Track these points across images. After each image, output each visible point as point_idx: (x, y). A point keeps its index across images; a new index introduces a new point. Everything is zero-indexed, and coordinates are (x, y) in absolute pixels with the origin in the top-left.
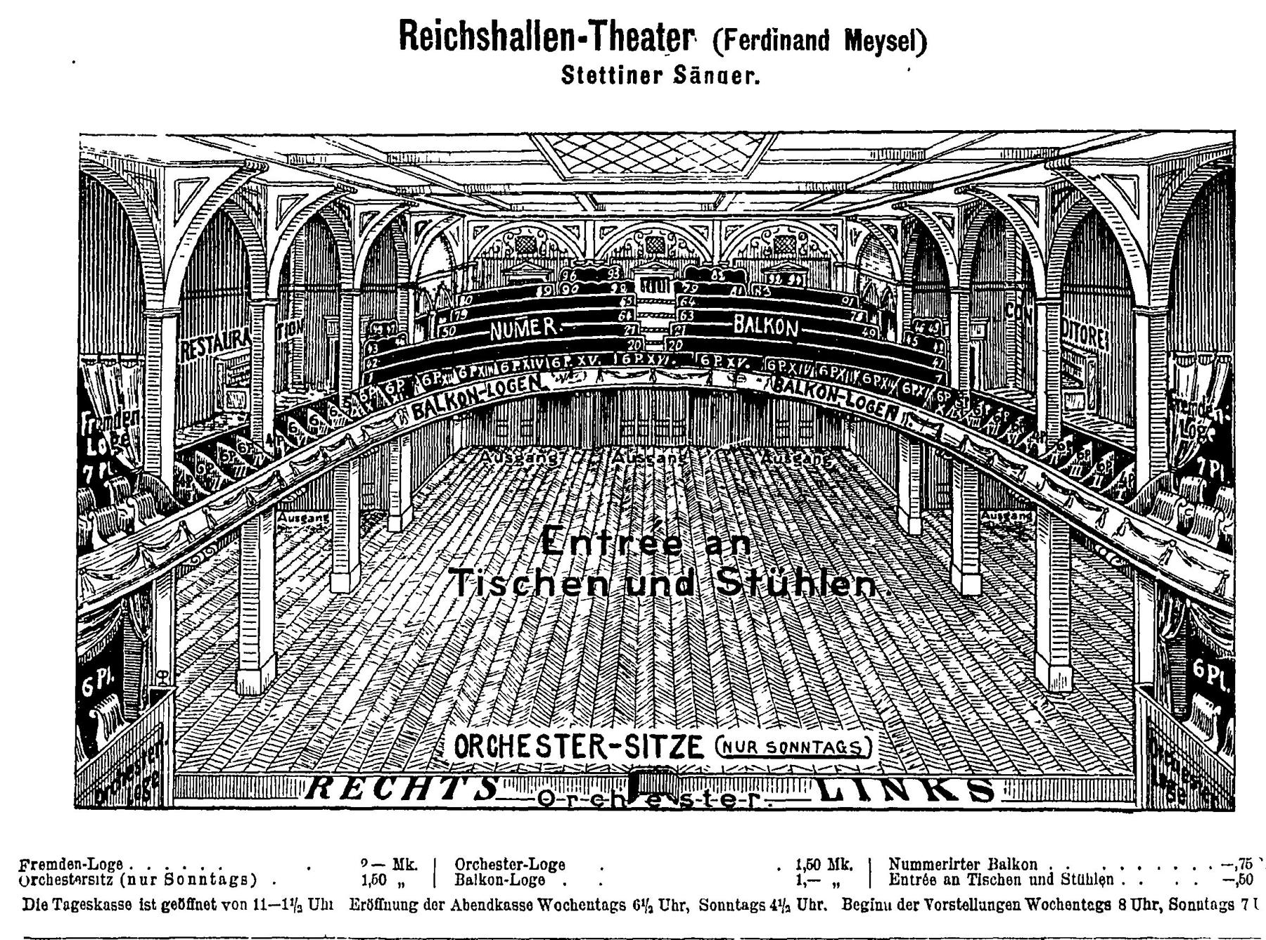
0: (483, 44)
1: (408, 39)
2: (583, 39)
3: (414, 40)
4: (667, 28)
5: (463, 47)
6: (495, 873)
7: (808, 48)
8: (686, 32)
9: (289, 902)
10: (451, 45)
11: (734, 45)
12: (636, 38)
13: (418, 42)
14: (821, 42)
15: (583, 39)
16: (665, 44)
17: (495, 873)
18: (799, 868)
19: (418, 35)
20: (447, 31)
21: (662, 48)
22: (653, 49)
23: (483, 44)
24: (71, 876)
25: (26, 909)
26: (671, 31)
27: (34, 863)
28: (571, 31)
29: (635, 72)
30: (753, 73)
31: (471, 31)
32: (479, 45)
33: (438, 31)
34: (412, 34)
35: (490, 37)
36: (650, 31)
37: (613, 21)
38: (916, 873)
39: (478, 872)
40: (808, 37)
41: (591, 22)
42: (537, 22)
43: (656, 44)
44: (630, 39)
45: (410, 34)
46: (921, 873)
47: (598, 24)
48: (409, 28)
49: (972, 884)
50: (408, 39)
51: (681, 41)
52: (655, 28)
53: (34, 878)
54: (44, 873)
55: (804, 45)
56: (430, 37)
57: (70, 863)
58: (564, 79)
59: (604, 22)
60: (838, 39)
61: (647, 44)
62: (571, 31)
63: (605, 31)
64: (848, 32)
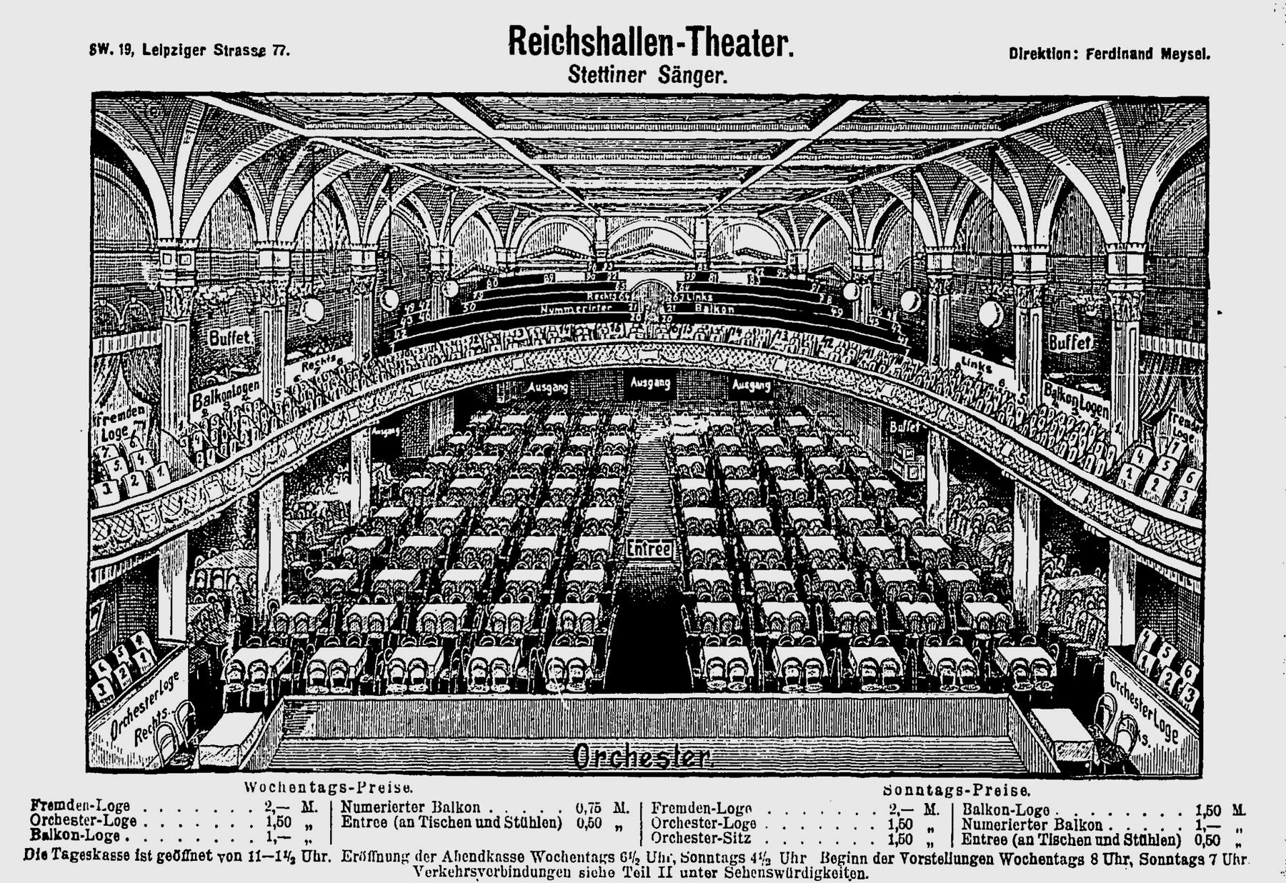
1: (517, 45)
2: (681, 45)
3: (522, 45)
4: (761, 35)
5: (569, 52)
7: (632, 54)
9: (282, 854)
11: (1092, 57)
12: (732, 43)
13: (526, 48)
14: (1149, 54)
15: (681, 45)
16: (760, 50)
19: (526, 40)
21: (757, 54)
22: (748, 54)
23: (588, 40)
26: (765, 37)
28: (670, 38)
30: (722, 73)
31: (576, 36)
32: (584, 51)
33: (547, 36)
34: (520, 40)
35: (595, 43)
36: (746, 38)
37: (709, 28)
38: (367, 816)
40: (662, 38)
41: (688, 28)
42: (640, 28)
43: (752, 50)
44: (724, 45)
46: (373, 815)
47: (695, 29)
48: (517, 33)
49: (423, 826)
50: (517, 45)
51: (658, 47)
52: (750, 34)
55: (627, 49)
58: (660, 79)
59: (701, 28)
60: (1157, 53)
61: (743, 50)
62: (670, 38)
63: (702, 36)
64: (1163, 50)
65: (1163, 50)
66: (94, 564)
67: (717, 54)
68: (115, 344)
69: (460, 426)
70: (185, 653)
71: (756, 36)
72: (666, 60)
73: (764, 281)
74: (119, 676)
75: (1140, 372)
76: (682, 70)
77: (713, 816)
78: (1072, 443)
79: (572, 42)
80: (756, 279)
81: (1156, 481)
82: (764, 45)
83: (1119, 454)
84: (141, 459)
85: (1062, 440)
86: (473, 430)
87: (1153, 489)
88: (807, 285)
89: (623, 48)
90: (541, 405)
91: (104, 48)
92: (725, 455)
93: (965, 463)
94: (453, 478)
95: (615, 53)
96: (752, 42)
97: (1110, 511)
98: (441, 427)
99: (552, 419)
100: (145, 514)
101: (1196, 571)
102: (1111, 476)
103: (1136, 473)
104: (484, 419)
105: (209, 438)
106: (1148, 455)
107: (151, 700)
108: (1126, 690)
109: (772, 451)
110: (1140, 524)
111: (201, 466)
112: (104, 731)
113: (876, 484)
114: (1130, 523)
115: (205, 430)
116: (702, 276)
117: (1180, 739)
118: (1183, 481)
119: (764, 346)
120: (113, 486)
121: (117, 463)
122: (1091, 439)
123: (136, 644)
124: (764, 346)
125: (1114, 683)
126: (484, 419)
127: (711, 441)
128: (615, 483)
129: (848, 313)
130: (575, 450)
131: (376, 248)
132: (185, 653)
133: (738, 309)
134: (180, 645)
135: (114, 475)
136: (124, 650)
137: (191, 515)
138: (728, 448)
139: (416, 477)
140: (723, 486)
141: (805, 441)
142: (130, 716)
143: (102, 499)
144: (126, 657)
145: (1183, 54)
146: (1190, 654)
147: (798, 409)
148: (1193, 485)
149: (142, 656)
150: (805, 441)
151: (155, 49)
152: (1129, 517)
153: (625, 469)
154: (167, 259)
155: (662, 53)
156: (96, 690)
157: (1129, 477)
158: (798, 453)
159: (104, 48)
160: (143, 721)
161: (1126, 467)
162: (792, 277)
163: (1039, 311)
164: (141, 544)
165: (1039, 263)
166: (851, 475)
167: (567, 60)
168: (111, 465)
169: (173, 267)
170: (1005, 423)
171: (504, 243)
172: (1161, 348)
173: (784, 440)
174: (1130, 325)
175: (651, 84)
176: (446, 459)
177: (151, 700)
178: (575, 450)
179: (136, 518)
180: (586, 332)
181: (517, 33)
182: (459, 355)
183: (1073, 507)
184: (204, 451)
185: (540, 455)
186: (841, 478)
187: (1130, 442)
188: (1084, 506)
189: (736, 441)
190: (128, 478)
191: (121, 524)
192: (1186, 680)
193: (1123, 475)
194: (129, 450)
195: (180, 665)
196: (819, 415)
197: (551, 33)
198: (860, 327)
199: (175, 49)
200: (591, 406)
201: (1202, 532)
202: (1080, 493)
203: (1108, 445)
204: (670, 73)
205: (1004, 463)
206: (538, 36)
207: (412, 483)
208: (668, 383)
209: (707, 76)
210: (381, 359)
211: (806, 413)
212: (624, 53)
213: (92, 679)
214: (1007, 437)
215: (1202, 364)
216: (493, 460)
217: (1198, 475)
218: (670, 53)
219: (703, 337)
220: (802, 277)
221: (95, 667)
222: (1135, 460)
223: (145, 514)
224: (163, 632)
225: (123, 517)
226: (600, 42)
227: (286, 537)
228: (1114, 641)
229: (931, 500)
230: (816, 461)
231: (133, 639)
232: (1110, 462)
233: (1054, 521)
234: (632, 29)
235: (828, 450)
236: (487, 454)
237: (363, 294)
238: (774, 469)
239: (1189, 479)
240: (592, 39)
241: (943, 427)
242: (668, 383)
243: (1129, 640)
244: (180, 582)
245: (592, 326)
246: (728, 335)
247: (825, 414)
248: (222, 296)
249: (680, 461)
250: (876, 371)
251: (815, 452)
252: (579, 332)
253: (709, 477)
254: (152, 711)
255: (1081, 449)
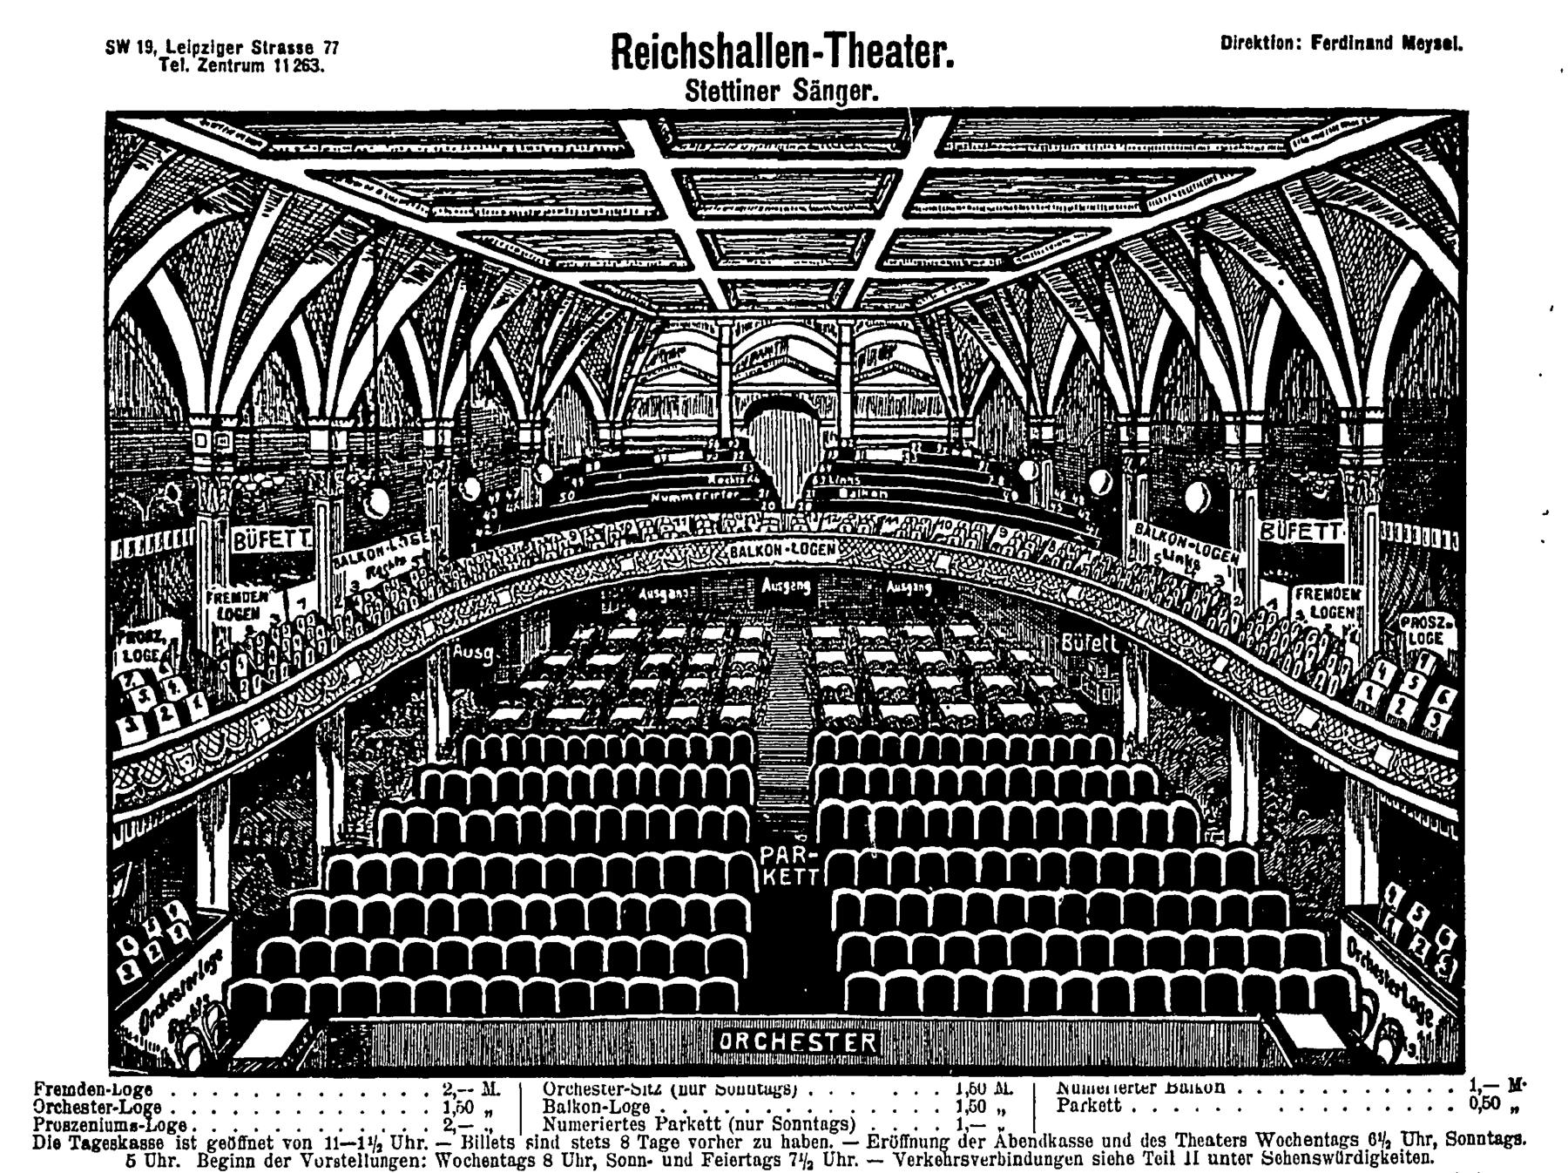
0: (707, 61)
1: (621, 57)
2: (818, 55)
3: (627, 56)
4: (915, 41)
5: (684, 66)
6: (591, 1099)
7: (759, 65)
8: (937, 45)
10: (670, 61)
11: (1320, 46)
12: (880, 52)
13: (633, 60)
14: (1388, 44)
15: (818, 55)
17: (591, 1099)
18: (960, 1093)
19: (632, 51)
20: (666, 46)
21: (910, 65)
23: (707, 61)
24: (94, 1103)
25: (36, 1147)
27: (49, 1087)
28: (805, 46)
29: (752, 87)
31: (692, 45)
32: (701, 62)
33: (655, 46)
34: (625, 51)
35: (714, 53)
36: (898, 45)
37: (853, 34)
39: (571, 1098)
40: (796, 45)
41: (827, 35)
42: (769, 35)
44: (871, 54)
45: (1227, 43)
47: (834, 36)
48: (622, 43)
50: (621, 57)
52: (902, 40)
53: (50, 1105)
54: (59, 1100)
55: (754, 60)
56: (646, 55)
57: (91, 1089)
59: (843, 34)
60: (1398, 42)
61: (894, 60)
62: (805, 46)
63: (844, 43)
64: (1405, 37)
65: (1405, 37)
66: (117, 818)
67: (769, 65)
68: (140, 545)
69: (559, 645)
70: (229, 929)
71: (909, 44)
72: (800, 72)
73: (921, 459)
74: (149, 954)
75: (1381, 568)
76: (821, 85)
77: (108, 1098)
78: (1297, 655)
79: (686, 51)
80: (912, 456)
81: (1402, 702)
82: (919, 54)
83: (1356, 668)
84: (172, 686)
85: (1286, 652)
86: (575, 648)
87: (1398, 712)
88: (973, 463)
89: (749, 58)
90: (654, 617)
91: (124, 46)
92: (878, 674)
93: (1173, 686)
94: (550, 708)
95: (740, 65)
96: (904, 50)
97: (1345, 739)
98: (535, 644)
99: (668, 633)
100: (179, 756)
101: (1451, 814)
102: (1346, 695)
103: (1377, 692)
104: (587, 634)
105: (255, 661)
106: (1391, 669)
107: (190, 983)
108: (1370, 962)
109: (934, 669)
110: (1384, 756)
111: (245, 696)
112: (132, 1023)
113: (1062, 708)
114: (1372, 753)
115: (251, 652)
116: (847, 453)
117: (1435, 1021)
118: (1434, 702)
119: (924, 539)
120: (139, 720)
121: (143, 693)
122: (1323, 650)
123: (171, 916)
124: (924, 539)
125: (1354, 953)
126: (587, 634)
127: (861, 657)
128: (745, 711)
129: (1025, 497)
130: (695, 670)
131: (452, 424)
132: (229, 929)
133: (892, 494)
134: (223, 916)
135: (139, 707)
136: (156, 923)
137: (233, 757)
138: (883, 665)
139: (505, 706)
140: (877, 712)
141: (975, 656)
142: (165, 1004)
143: (126, 738)
144: (157, 932)
145: (1429, 43)
146: (1448, 904)
147: (963, 617)
148: (1446, 707)
149: (178, 930)
150: (975, 656)
151: (181, 46)
152: (1370, 747)
153: (758, 693)
154: (201, 441)
155: (796, 65)
156: (121, 972)
157: (1369, 697)
158: (965, 670)
159: (124, 46)
160: (180, 1011)
161: (1366, 684)
162: (955, 452)
163: (1254, 493)
164: (174, 793)
165: (1254, 434)
166: (1032, 697)
167: (681, 75)
168: (136, 695)
169: (208, 450)
170: (1216, 631)
171: (607, 415)
172: (1405, 537)
173: (948, 655)
174: (1368, 510)
175: (785, 100)
176: (541, 685)
177: (190, 983)
178: (695, 670)
179: (168, 760)
180: (707, 524)
181: (622, 43)
182: (555, 555)
183: (1301, 735)
184: (249, 677)
185: (653, 677)
186: (1019, 701)
187: (1370, 653)
188: (1314, 734)
189: (891, 656)
190: (157, 710)
191: (150, 767)
192: (1442, 947)
193: (1361, 695)
194: (159, 676)
195: (223, 941)
196: (990, 624)
197: (661, 42)
198: (1040, 514)
199: (206, 46)
200: (716, 616)
201: (1459, 766)
202: (1308, 717)
203: (1342, 657)
204: (808, 88)
205: (1216, 681)
206: (645, 46)
207: (501, 714)
208: (807, 585)
209: (852, 92)
210: (461, 561)
211: (975, 623)
212: (750, 65)
213: (115, 958)
214: (1220, 647)
215: (1457, 562)
216: (598, 684)
217: (1452, 695)
218: (805, 64)
219: (849, 528)
220: (967, 453)
221: (120, 944)
222: (1376, 676)
223: (179, 756)
224: (203, 900)
225: (153, 759)
226: (724, 51)
227: (349, 782)
228: (1352, 898)
229: (1129, 727)
230: (989, 681)
231: (167, 908)
232: (1344, 678)
233: (1276, 753)
234: (759, 35)
235: (1002, 667)
236: (589, 678)
237: (438, 482)
238: (936, 691)
239: (1442, 699)
240: (711, 48)
241: (1142, 637)
242: (807, 585)
243: (1372, 898)
244: (222, 838)
245: (715, 517)
246: (879, 525)
247: (997, 624)
248: (267, 485)
249: (824, 682)
250: (1060, 567)
251: (987, 669)
252: (699, 524)
253: (858, 702)
254: (190, 998)
255: (1309, 661)
